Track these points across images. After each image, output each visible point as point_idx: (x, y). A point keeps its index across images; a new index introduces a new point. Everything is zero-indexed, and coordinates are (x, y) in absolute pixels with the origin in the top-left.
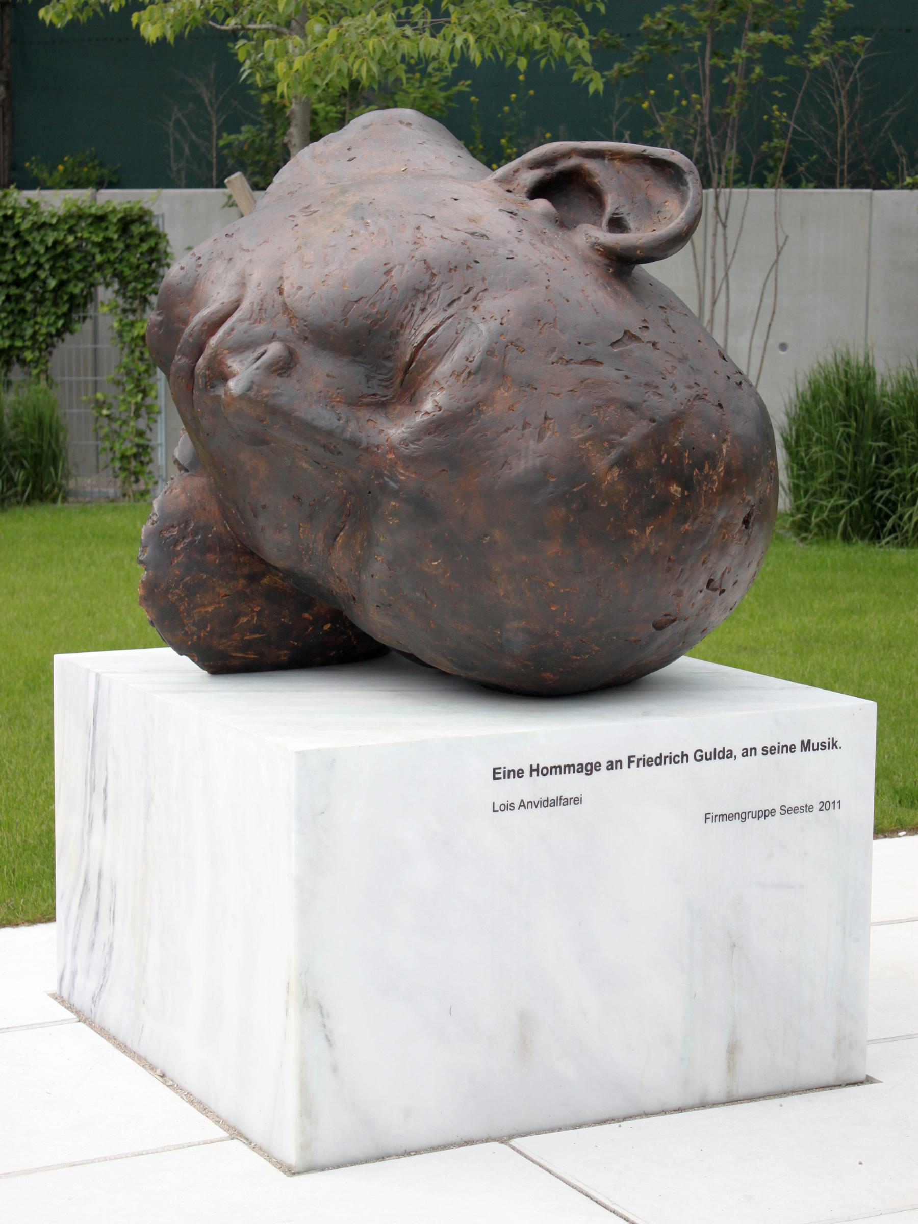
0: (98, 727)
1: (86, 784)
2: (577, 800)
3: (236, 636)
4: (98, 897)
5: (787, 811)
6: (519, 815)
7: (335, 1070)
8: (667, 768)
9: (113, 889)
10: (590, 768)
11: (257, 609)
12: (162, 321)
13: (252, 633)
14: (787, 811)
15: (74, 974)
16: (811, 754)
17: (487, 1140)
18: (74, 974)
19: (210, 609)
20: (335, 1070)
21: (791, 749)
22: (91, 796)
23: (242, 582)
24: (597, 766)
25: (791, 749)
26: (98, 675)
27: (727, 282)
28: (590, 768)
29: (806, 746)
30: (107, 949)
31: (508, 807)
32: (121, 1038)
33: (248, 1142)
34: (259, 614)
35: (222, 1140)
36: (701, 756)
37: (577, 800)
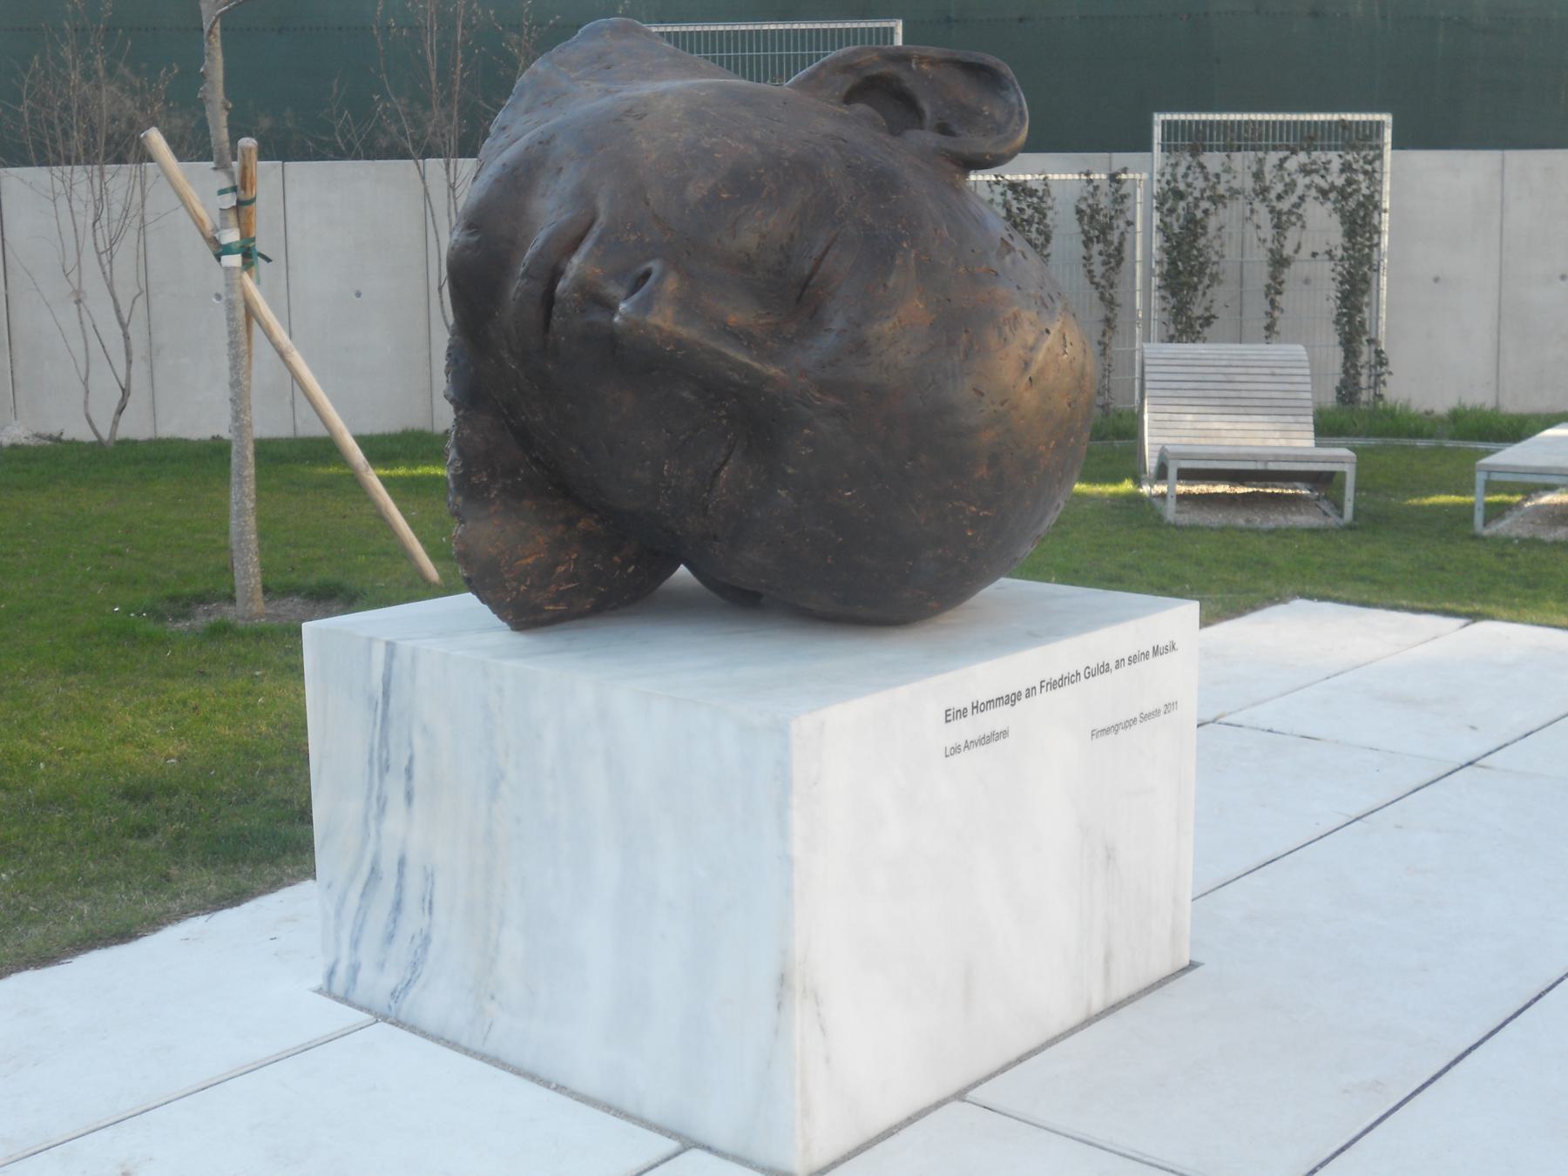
0: (392, 701)
1: (371, 762)
2: (1005, 733)
3: (553, 588)
4: (400, 887)
5: (1145, 717)
6: (965, 754)
7: (828, 1060)
8: (1068, 688)
9: (429, 877)
10: (1012, 699)
11: (574, 556)
12: (478, 242)
13: (568, 582)
14: (1145, 717)
15: (355, 969)
16: (1159, 658)
17: (939, 1105)
18: (355, 969)
19: (530, 561)
20: (828, 1060)
21: (1146, 655)
22: (381, 777)
23: (561, 527)
24: (1017, 696)
25: (1146, 655)
26: (391, 647)
27: (120, 319)
28: (1012, 699)
29: (1156, 651)
30: (418, 941)
31: (956, 750)
32: (448, 1037)
33: (709, 1149)
34: (576, 561)
35: (677, 1154)
36: (1090, 673)
37: (1005, 733)
